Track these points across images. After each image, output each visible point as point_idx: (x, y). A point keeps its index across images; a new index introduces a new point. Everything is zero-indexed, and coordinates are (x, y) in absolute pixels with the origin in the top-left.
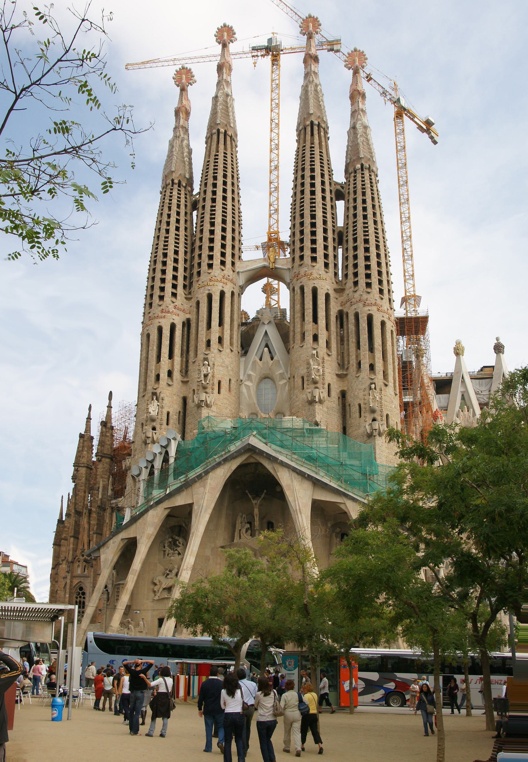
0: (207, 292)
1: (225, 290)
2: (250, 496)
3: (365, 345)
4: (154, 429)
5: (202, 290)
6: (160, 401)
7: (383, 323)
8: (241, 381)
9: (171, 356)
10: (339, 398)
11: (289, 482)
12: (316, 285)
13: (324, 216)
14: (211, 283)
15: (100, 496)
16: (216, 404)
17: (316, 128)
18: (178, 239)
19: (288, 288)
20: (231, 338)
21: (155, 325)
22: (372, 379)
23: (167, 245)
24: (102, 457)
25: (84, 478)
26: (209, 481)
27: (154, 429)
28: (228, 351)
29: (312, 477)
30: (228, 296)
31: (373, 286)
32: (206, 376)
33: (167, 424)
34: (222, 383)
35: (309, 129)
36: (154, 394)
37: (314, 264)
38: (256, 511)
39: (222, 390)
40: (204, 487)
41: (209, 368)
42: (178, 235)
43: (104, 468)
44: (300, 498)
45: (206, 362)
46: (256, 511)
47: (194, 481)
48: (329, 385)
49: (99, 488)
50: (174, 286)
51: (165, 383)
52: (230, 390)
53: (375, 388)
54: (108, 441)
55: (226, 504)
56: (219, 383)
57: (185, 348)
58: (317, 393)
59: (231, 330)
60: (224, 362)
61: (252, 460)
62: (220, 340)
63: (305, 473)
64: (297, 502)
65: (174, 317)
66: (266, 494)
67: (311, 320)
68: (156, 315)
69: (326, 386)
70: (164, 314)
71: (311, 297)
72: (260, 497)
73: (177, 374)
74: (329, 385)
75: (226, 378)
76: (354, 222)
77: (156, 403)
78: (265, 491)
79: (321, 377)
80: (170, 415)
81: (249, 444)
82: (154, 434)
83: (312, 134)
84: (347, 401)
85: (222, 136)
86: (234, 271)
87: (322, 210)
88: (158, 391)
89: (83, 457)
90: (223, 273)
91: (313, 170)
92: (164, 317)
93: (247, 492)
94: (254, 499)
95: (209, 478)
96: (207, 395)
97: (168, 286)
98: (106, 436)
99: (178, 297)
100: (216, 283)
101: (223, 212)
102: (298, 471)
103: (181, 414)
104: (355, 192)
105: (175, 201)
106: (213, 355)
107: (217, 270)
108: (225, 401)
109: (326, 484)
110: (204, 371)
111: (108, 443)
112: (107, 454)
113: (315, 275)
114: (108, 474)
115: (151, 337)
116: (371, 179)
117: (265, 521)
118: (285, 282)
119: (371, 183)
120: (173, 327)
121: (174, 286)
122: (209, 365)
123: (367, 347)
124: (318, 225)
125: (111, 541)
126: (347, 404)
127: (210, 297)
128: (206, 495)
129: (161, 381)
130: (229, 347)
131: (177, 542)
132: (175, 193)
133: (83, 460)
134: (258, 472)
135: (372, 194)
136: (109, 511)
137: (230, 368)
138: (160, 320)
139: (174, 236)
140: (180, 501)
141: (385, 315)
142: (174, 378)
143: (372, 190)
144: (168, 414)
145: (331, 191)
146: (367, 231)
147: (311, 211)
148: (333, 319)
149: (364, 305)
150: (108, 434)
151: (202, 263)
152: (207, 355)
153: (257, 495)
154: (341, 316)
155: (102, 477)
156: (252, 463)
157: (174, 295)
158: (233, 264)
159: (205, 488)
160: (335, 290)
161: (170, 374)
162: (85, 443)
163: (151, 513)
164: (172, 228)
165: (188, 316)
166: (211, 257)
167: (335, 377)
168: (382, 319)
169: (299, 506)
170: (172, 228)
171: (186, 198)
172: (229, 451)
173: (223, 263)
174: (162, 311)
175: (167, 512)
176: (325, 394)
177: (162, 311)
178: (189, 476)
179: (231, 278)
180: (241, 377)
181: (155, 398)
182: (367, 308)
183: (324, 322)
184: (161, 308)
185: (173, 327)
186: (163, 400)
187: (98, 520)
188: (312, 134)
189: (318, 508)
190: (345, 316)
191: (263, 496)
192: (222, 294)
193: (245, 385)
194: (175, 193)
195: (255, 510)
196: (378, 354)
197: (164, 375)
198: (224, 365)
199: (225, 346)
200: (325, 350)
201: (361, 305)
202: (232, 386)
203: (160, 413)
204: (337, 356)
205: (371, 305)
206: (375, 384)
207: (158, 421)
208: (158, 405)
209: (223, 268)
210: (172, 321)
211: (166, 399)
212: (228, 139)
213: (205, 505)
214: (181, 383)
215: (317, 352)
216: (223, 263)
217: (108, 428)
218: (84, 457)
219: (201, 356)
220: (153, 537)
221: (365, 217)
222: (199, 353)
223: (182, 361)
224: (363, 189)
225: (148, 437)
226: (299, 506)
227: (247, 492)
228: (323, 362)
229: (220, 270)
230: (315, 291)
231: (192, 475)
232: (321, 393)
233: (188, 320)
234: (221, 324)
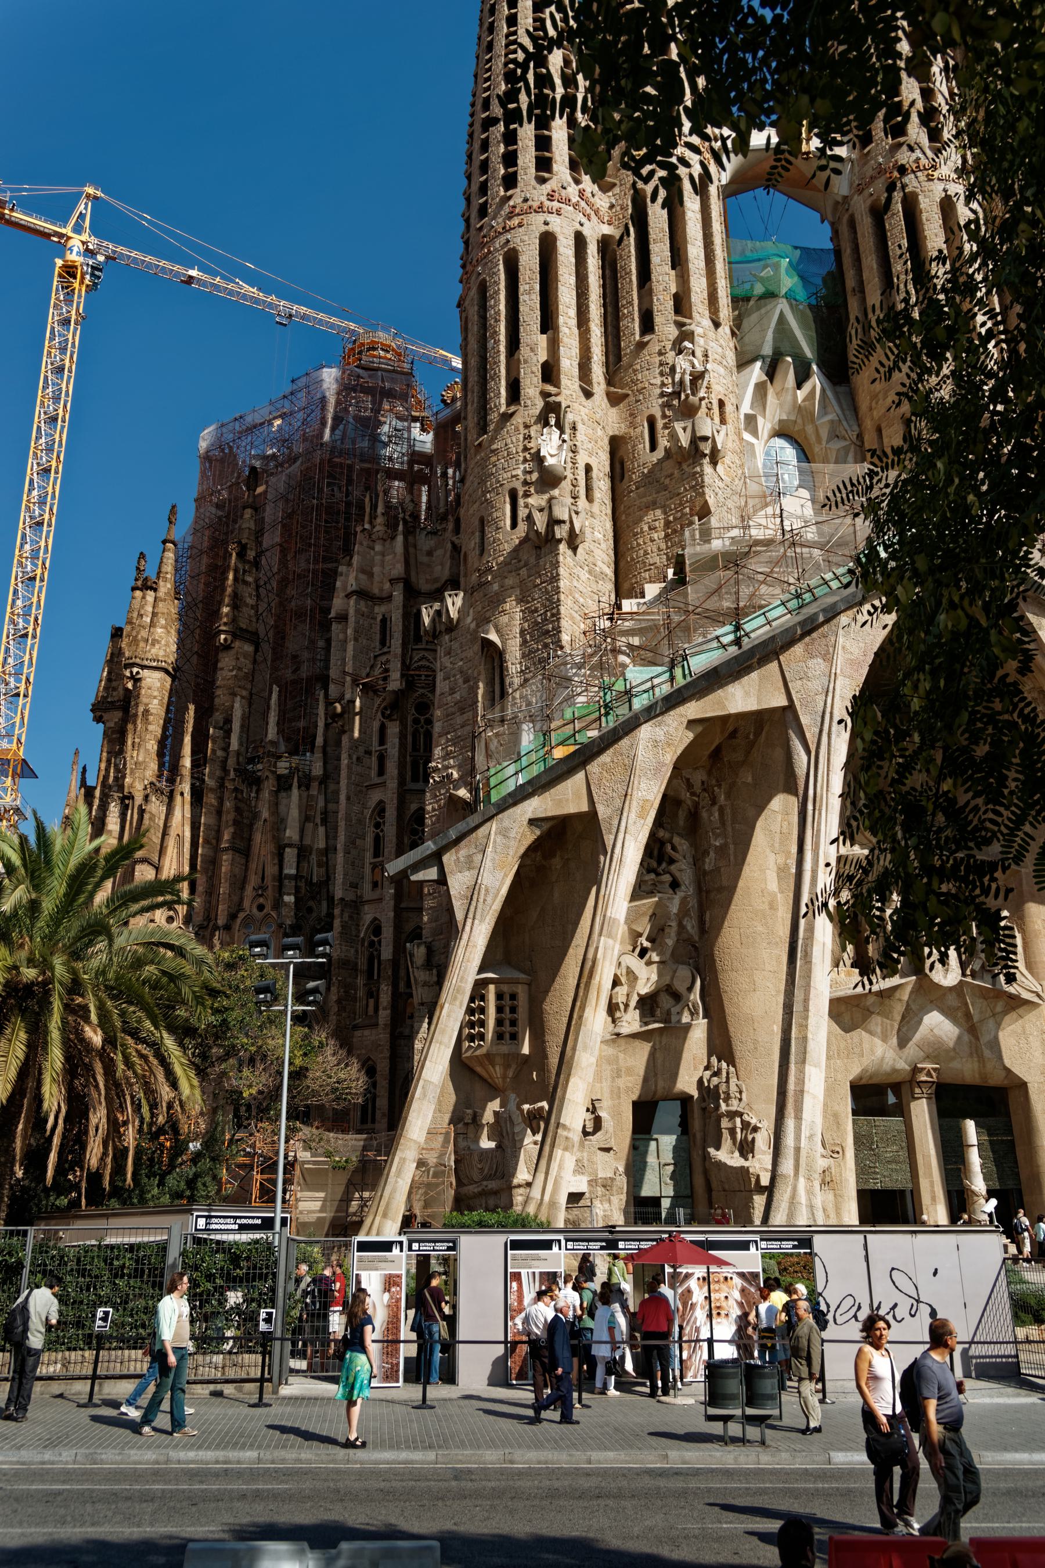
1: (586, 231)
21: (534, 228)
25: (156, 702)
30: (566, 252)
40: (829, 658)
68: (535, 205)
70: (555, 205)
92: (520, 225)
98: (245, 583)
112: (246, 631)
131: (669, 847)
133: (154, 651)
136: (269, 786)
150: (250, 579)
162: (161, 604)
163: (646, 732)
174: (551, 197)
177: (551, 197)
181: (553, 422)
207: (566, 485)
217: (249, 562)
218: (159, 642)
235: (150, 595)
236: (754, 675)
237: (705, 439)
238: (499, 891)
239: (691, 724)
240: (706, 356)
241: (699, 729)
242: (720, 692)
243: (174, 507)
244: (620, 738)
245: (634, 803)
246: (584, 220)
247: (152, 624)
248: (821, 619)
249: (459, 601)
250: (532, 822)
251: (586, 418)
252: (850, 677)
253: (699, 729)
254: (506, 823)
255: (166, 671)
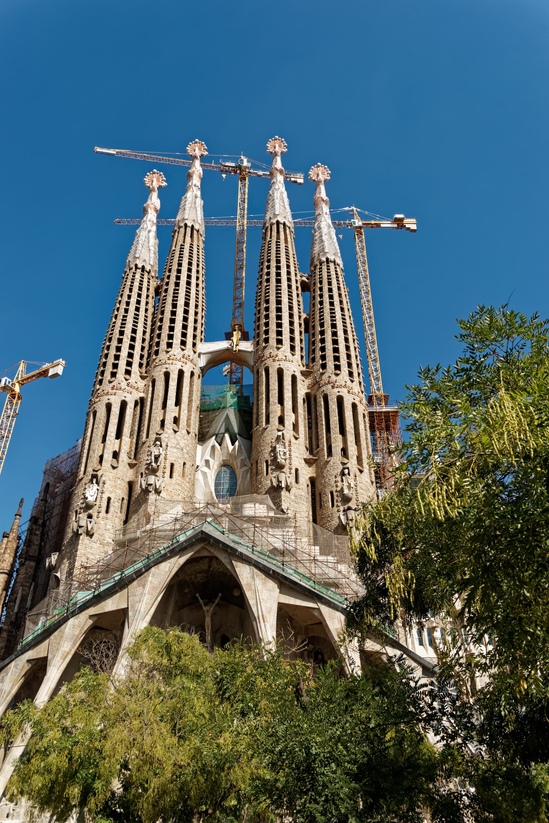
0: (164, 370)
2: (201, 601)
3: (336, 427)
4: (90, 517)
5: (158, 368)
6: (101, 484)
7: (354, 406)
8: (198, 467)
9: (119, 435)
10: (308, 485)
11: (250, 580)
12: (281, 366)
13: (289, 302)
14: (170, 362)
15: (16, 610)
16: (167, 490)
17: (281, 226)
18: (138, 319)
19: (252, 371)
20: (189, 419)
22: (345, 464)
23: (125, 324)
24: (26, 559)
26: (150, 578)
27: (90, 517)
28: (185, 432)
29: (278, 574)
30: (187, 375)
31: (342, 368)
32: (157, 458)
33: (107, 512)
34: (175, 467)
35: (275, 227)
36: (94, 476)
37: (280, 346)
38: (208, 620)
39: (175, 475)
41: (161, 449)
42: (138, 315)
43: (27, 574)
44: (264, 599)
45: (158, 443)
46: (208, 620)
47: (131, 580)
48: (297, 470)
49: (16, 599)
50: (129, 364)
51: (109, 465)
52: (183, 475)
53: (349, 474)
54: (37, 540)
55: (170, 611)
56: (172, 465)
57: (136, 428)
58: (282, 477)
59: (189, 410)
60: (178, 444)
61: (205, 553)
62: (176, 421)
63: (269, 569)
64: (259, 607)
65: (126, 394)
66: (220, 598)
67: (277, 401)
68: (105, 392)
69: (293, 471)
70: (114, 391)
71: (277, 378)
72: (214, 603)
73: (124, 457)
74: (297, 470)
75: (179, 461)
76: (320, 309)
77: (95, 486)
78: (220, 595)
79: (288, 461)
80: (112, 501)
81: (202, 532)
82: (89, 523)
83: (278, 232)
84: (316, 490)
85: (189, 230)
86: (195, 352)
87: (287, 296)
88: (99, 473)
89: (4, 560)
90: (182, 353)
91: (278, 261)
92: (115, 394)
93: (197, 595)
94: (206, 605)
95: (151, 575)
96: (157, 478)
97: (122, 364)
98: (36, 535)
99: (132, 375)
100: (174, 362)
101: (186, 295)
102: (261, 566)
103: (126, 502)
104: (321, 282)
105: (136, 284)
106: (167, 435)
107: (176, 349)
108: (177, 487)
109: (296, 583)
110: (155, 451)
111: (36, 543)
113: (280, 356)
114: (31, 581)
115: (98, 414)
116: (336, 271)
117: (219, 635)
118: (248, 365)
119: (337, 274)
120: (124, 405)
121: (129, 364)
122: (161, 446)
123: (338, 429)
124: (283, 310)
125: (13, 664)
126: (317, 493)
127: (167, 375)
128: (146, 597)
129: (104, 463)
130: (186, 427)
132: (138, 276)
134: (212, 569)
135: (338, 284)
137: (185, 451)
138: (110, 397)
139: (133, 315)
140: (110, 605)
141: (356, 397)
142: (120, 459)
143: (338, 280)
144: (109, 499)
145: (297, 281)
146: (335, 317)
147: (277, 297)
148: (300, 401)
149: (333, 387)
150: (38, 533)
151: (161, 342)
152: (160, 435)
153: (209, 600)
154: (309, 399)
155: (22, 586)
156: (206, 557)
157: (128, 372)
158: (194, 345)
159: (144, 587)
160: (302, 373)
161: (116, 455)
164: (132, 308)
165: (142, 395)
166: (171, 337)
167: (303, 462)
168: (354, 401)
169: (262, 611)
170: (132, 308)
171: (149, 282)
172: (178, 542)
173: (183, 343)
174: (169, 359)
175: (90, 622)
176: (292, 480)
177: (169, 359)
178: (126, 573)
179: (191, 358)
180: (198, 463)
182: (336, 390)
183: (290, 403)
184: (112, 384)
185: (124, 405)
186: (104, 483)
187: (8, 641)
188: (278, 232)
189: (284, 614)
190: (312, 399)
191: (217, 601)
192: (181, 373)
193: (202, 471)
194: (138, 276)
195: (207, 619)
196: (351, 438)
197: (108, 456)
198: (178, 446)
199: (180, 426)
200: (292, 432)
201: (329, 386)
202: (186, 470)
203: (99, 499)
204: (306, 440)
205: (340, 386)
206: (348, 468)
207: (96, 508)
208: (98, 490)
209: (183, 347)
210: (124, 398)
211: (108, 483)
212: (195, 232)
213: (142, 610)
214: (127, 466)
215: (283, 434)
216: (183, 343)
219: (153, 436)
220: (70, 657)
221: (332, 304)
222: (150, 432)
223: (131, 442)
224: (328, 279)
225: (81, 527)
226: (262, 611)
227: (197, 595)
228: (290, 445)
229: (180, 350)
230: (280, 372)
231: (129, 571)
232: (286, 477)
233: (142, 400)
234: (178, 403)
235: (6, 539)
236: (118, 595)
237: (151, 485)
238: (10, 692)
239: (91, 617)
240: (167, 446)
241: (96, 618)
242: (103, 603)
243: (22, 501)
244: (62, 625)
245: (60, 653)
246: (183, 365)
247: (4, 553)
248: (144, 570)
249: (56, 557)
250: (28, 661)
251: (111, 478)
252: (152, 594)
253: (96, 618)
254: (18, 662)
255: (6, 573)
